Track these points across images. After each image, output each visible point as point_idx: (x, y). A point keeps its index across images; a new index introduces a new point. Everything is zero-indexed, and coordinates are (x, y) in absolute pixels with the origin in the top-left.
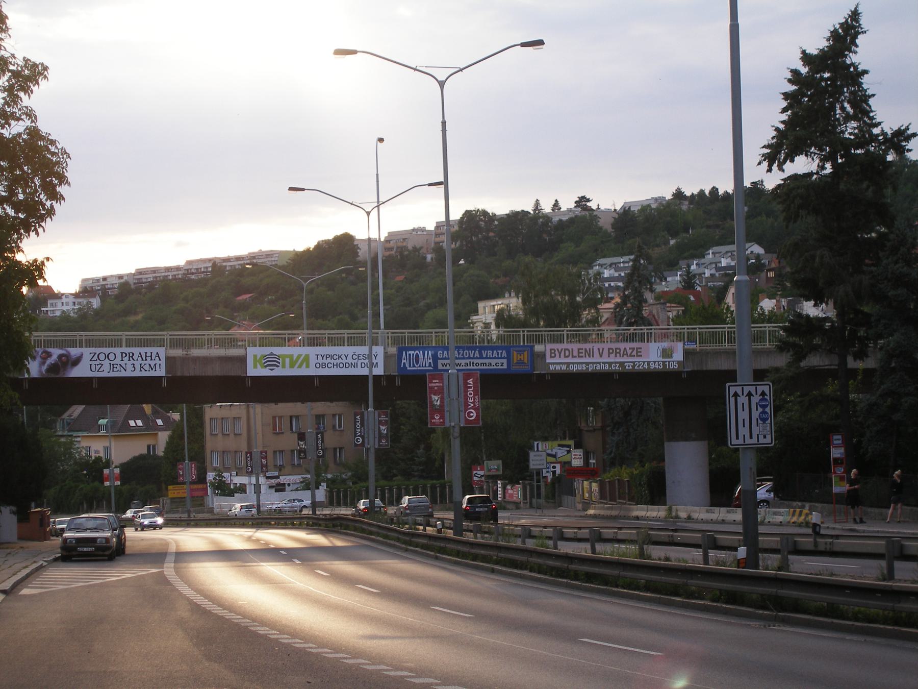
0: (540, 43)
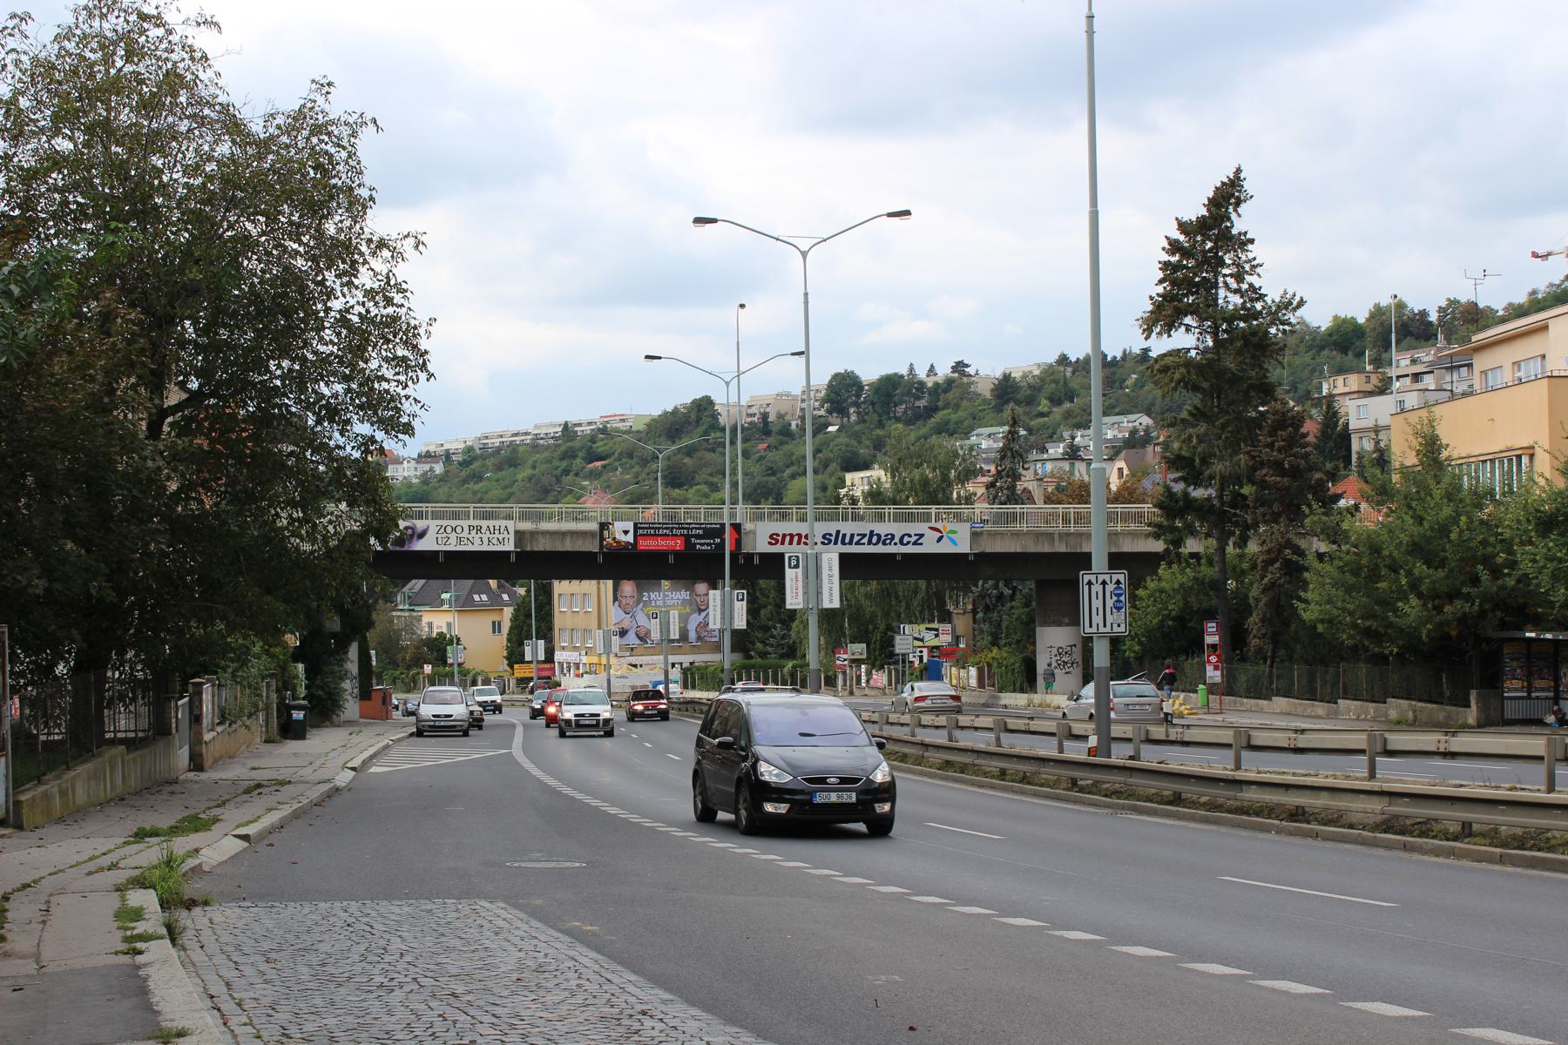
0: (907, 213)
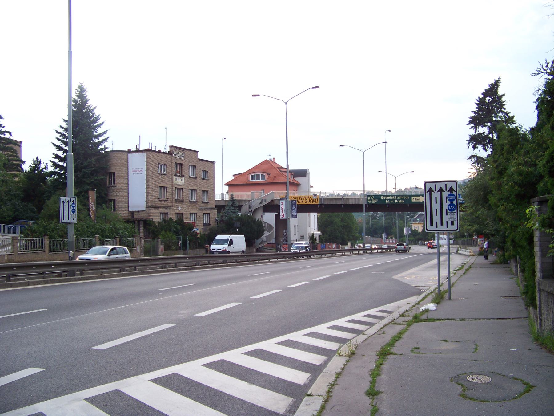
0: (253, 96)
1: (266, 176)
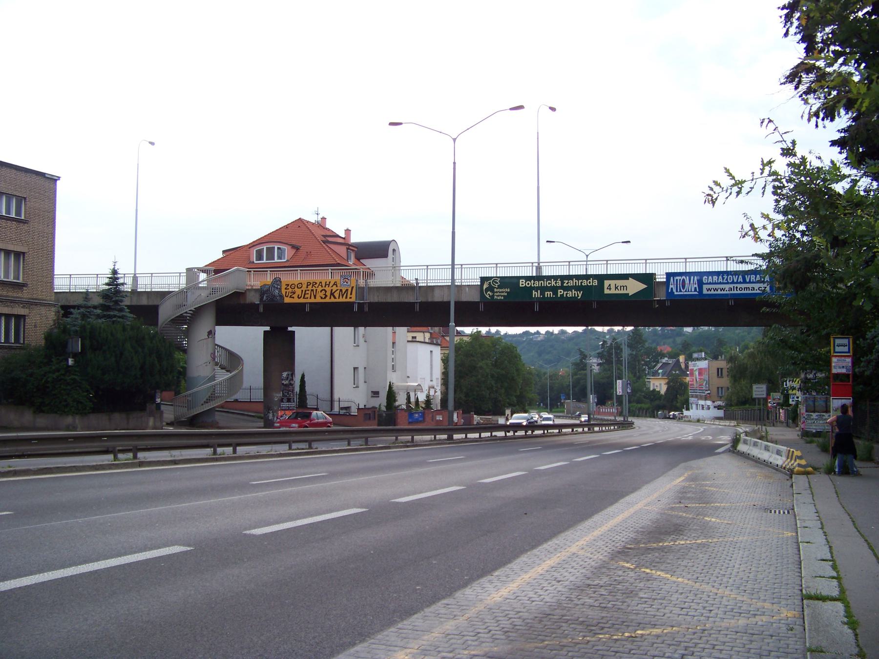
1: (288, 252)
